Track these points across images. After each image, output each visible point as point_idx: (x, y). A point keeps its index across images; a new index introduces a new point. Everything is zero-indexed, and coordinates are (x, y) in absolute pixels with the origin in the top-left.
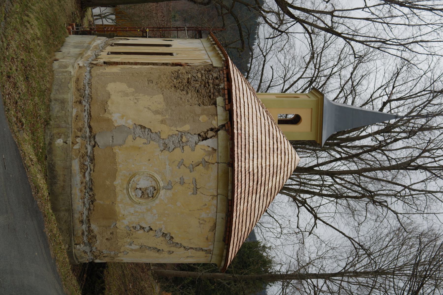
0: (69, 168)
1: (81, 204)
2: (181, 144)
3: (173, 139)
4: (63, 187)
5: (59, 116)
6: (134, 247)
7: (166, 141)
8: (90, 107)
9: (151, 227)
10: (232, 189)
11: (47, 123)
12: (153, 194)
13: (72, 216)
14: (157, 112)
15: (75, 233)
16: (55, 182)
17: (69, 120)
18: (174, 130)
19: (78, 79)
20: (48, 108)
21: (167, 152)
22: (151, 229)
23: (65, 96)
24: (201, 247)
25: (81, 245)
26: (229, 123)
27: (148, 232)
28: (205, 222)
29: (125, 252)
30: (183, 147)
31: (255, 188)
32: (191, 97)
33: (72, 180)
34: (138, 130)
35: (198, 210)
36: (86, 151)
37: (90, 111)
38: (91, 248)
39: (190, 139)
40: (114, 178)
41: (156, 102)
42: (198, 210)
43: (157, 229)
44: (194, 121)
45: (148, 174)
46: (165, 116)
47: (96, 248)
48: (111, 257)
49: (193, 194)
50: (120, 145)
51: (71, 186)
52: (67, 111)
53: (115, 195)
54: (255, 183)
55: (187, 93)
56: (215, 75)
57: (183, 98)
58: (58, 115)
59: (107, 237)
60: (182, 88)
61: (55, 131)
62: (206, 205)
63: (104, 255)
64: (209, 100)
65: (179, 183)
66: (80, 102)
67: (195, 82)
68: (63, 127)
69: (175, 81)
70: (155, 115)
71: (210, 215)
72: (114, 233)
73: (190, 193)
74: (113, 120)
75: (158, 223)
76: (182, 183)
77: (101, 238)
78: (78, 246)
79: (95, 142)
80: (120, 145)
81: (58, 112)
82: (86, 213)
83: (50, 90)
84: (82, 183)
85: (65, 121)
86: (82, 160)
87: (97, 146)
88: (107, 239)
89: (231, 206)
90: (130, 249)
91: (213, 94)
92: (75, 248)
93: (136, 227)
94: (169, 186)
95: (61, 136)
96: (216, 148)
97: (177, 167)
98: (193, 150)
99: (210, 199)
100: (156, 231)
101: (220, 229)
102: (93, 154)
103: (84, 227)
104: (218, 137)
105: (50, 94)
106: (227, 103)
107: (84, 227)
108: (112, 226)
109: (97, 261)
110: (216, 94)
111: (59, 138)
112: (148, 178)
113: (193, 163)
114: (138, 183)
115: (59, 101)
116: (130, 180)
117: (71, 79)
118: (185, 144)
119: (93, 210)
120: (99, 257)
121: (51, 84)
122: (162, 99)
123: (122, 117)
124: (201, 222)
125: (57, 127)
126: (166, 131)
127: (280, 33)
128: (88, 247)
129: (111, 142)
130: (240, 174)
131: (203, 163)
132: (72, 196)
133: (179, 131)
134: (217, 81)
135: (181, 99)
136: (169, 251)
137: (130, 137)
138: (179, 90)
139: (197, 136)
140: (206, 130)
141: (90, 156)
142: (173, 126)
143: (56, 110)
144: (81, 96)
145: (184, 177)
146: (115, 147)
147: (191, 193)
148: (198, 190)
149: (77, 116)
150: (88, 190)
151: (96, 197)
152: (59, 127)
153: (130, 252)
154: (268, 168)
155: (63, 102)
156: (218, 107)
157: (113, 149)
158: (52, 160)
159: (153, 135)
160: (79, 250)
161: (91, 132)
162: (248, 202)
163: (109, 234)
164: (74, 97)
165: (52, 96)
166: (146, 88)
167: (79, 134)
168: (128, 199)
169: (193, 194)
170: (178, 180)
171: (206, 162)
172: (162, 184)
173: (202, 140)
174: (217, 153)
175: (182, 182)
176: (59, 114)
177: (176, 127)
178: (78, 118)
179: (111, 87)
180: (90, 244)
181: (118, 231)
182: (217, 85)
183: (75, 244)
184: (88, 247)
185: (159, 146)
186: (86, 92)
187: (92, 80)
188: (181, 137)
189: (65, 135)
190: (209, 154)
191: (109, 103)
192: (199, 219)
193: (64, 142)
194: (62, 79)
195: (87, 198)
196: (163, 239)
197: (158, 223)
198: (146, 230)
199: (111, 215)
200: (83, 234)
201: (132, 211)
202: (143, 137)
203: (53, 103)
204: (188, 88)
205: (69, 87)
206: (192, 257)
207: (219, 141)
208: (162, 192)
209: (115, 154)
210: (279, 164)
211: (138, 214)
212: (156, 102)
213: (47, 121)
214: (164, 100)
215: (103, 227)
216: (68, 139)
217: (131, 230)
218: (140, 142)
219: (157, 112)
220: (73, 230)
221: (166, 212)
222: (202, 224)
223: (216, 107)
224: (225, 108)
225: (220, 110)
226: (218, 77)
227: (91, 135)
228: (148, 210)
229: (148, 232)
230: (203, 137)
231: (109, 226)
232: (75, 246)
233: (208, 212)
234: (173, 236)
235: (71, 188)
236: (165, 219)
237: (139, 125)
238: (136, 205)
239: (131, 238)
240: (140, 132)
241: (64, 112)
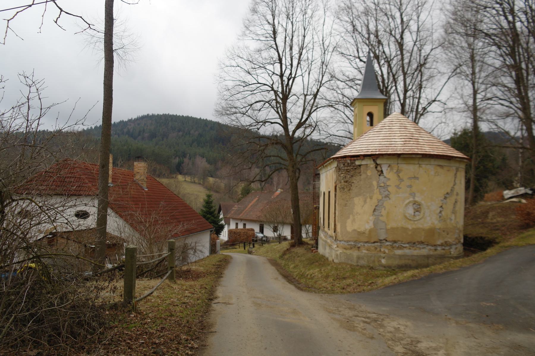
0: (400, 257)
2: (386, 187)
4: (413, 260)
6: (453, 218)
14: (365, 202)
18: (376, 191)
19: (345, 249)
22: (441, 207)
23: (355, 256)
34: (376, 213)
50: (386, 224)
55: (353, 183)
61: (377, 264)
66: (359, 248)
79: (384, 240)
82: (429, 247)
83: (351, 265)
84: (410, 249)
88: (448, 234)
94: (413, 194)
96: (388, 165)
98: (389, 179)
103: (439, 248)
109: (462, 241)
116: (409, 219)
122: (357, 198)
123: (368, 222)
126: (377, 196)
134: (346, 164)
137: (381, 218)
150: (414, 245)
152: (374, 261)
155: (359, 258)
159: (380, 204)
167: (378, 249)
170: (408, 189)
172: (411, 199)
175: (410, 186)
180: (450, 245)
188: (381, 186)
190: (392, 169)
191: (359, 230)
196: (448, 200)
199: (431, 232)
200: (443, 249)
208: (417, 199)
218: (384, 212)
219: (365, 202)
224: (363, 159)
225: (364, 162)
234: (446, 192)
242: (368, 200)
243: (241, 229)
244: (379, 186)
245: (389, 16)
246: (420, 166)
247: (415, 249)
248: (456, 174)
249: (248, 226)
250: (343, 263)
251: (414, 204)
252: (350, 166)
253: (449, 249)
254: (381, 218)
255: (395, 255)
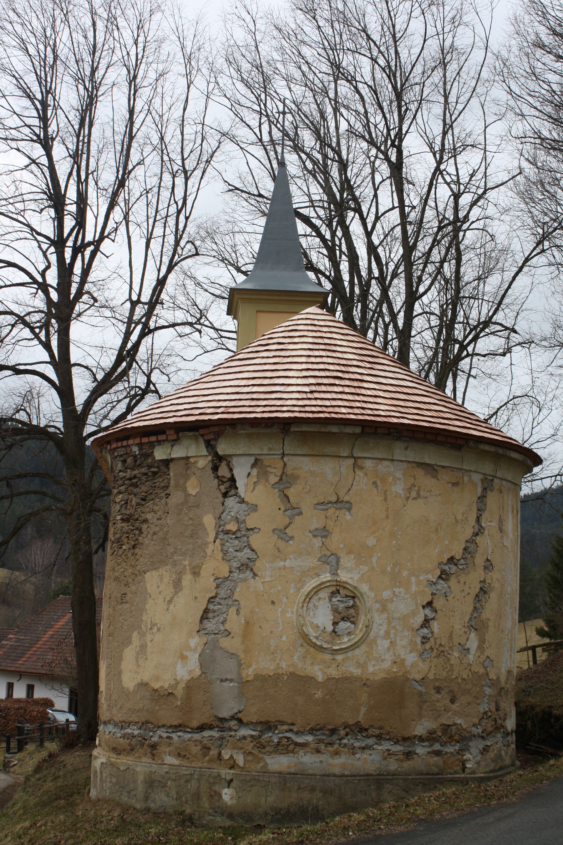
0: (285, 779)
1: (365, 756)
2: (243, 533)
3: (231, 550)
4: (327, 792)
5: (177, 793)
6: (473, 643)
7: (235, 564)
8: (163, 726)
9: (425, 603)
10: (338, 424)
11: (188, 821)
12: (347, 596)
13: (394, 775)
14: (177, 585)
15: (436, 770)
16: (313, 809)
17: (185, 772)
18: (214, 549)
19: (114, 750)
20: (158, 815)
21: (258, 563)
22: (430, 604)
23: (141, 778)
24: (475, 499)
25: (465, 758)
26: (202, 431)
27: (436, 611)
28: (413, 485)
29: (486, 664)
30: (248, 530)
31: (348, 383)
32: (153, 514)
33: (311, 772)
34: (209, 625)
35: (386, 500)
36: (249, 739)
37: (171, 727)
38: (474, 736)
39: (232, 514)
40: (309, 679)
41: (158, 587)
42: (386, 500)
43: (428, 591)
44: (198, 506)
45: (303, 606)
46: (185, 566)
47: (474, 725)
48: (499, 693)
49: (349, 510)
50: (240, 665)
51: (324, 775)
52: (168, 776)
53: (346, 679)
54: (337, 382)
55: (146, 521)
56: (120, 466)
57: (154, 529)
58: (175, 796)
59: (447, 701)
60: (137, 532)
61: (206, 804)
62: (374, 483)
63: (494, 710)
64: (160, 476)
65: (324, 540)
66: (154, 746)
67: (129, 507)
68: (199, 787)
69: (124, 547)
70: (182, 589)
71: (399, 475)
72: (437, 684)
73: (348, 517)
74: (189, 678)
75: (414, 588)
76: (324, 533)
77: (450, 714)
78: (468, 765)
79: (233, 718)
80: (240, 665)
81: (168, 796)
82: (386, 745)
83: (126, 809)
84: (318, 751)
85: (187, 781)
86: (268, 749)
87: (240, 715)
88: (452, 701)
89: (376, 428)
90: (479, 653)
91: (150, 467)
92: (474, 773)
93: (424, 637)
94: (331, 560)
95: (215, 792)
96: (252, 460)
97: (291, 542)
98: (254, 508)
99: (362, 475)
100: (433, 594)
101: (430, 455)
102: (256, 723)
103: (420, 750)
104: (230, 456)
105: (135, 809)
106: (163, 437)
107: (420, 750)
108: (419, 688)
109: (511, 724)
110: (150, 460)
111: (220, 795)
112: (311, 605)
113: (283, 508)
114: (322, 628)
115: (149, 791)
116: (314, 646)
117: (112, 764)
118: (242, 526)
119: (381, 728)
120: (499, 722)
121: (119, 804)
122: (154, 573)
123: (183, 658)
124: (414, 494)
125: (198, 799)
126: (214, 565)
127: (151, 386)
128: (471, 744)
129: (232, 684)
130: (307, 409)
131: (282, 487)
132: (346, 773)
133: (216, 538)
134: (129, 460)
135: (155, 534)
136: (486, 568)
137: (225, 642)
138: (140, 538)
139: (226, 499)
140: (216, 480)
141: (261, 731)
142: (204, 551)
143: (166, 799)
144: (142, 745)
145: (313, 528)
146: (244, 676)
147: (347, 513)
148: (341, 499)
149: (179, 754)
150: (335, 737)
151: (351, 722)
152: (197, 796)
153: (486, 654)
154: (313, 360)
155: (151, 783)
156: (174, 456)
157: (248, 681)
158: (266, 814)
159: (223, 593)
160: (478, 763)
161: (211, 727)
162: (376, 396)
163: (439, 696)
164: (144, 759)
165: (138, 806)
166: (133, 608)
167: (214, 752)
168: (357, 652)
169: (349, 510)
170: (317, 542)
171: (281, 479)
172: (326, 577)
173: (237, 488)
174: (262, 457)
175: (323, 533)
176: (173, 793)
177: (207, 544)
178: (183, 753)
179: (129, 681)
180: (463, 739)
181: (431, 676)
182: (136, 461)
183: (464, 771)
184: (471, 744)
185: (245, 580)
186: (136, 732)
187: (116, 719)
188: (227, 532)
189: (214, 783)
190: (264, 474)
191: (156, 686)
192: (408, 498)
193: (229, 787)
194: (111, 782)
195: (352, 741)
196: (453, 581)
197: (414, 588)
198: (430, 615)
199: (394, 691)
200: (438, 753)
201: (386, 643)
202: (225, 615)
203: (152, 805)
204: (137, 519)
205: (125, 768)
206: (501, 521)
207: (238, 453)
208: (344, 576)
209: (258, 677)
210: (310, 340)
211: (393, 631)
212: (158, 587)
213: (184, 821)
214: (155, 569)
215: (421, 707)
216: (223, 777)
217: (431, 648)
218: (234, 622)
219: (177, 585)
220: (428, 774)
221: (389, 569)
222: (418, 494)
223: (172, 460)
224: (176, 441)
225: (178, 452)
226: (122, 459)
227: (217, 726)
228: (384, 609)
229: (436, 611)
230: (230, 487)
231: (420, 694)
232: (467, 771)
233: (391, 479)
234: (446, 557)
235: (328, 776)
236: (405, 573)
237: (201, 622)
238: (372, 634)
239: (451, 648)
240: (214, 621)
241: (169, 783)
242: (187, 579)
243: (19, 701)
244: (222, 532)
245: (309, 43)
246: (355, 465)
247: (337, 753)
248: (482, 498)
249: (40, 693)
250: (106, 801)
251: (333, 594)
252: (140, 466)
253: (461, 752)
254: (225, 642)
255: (265, 771)
